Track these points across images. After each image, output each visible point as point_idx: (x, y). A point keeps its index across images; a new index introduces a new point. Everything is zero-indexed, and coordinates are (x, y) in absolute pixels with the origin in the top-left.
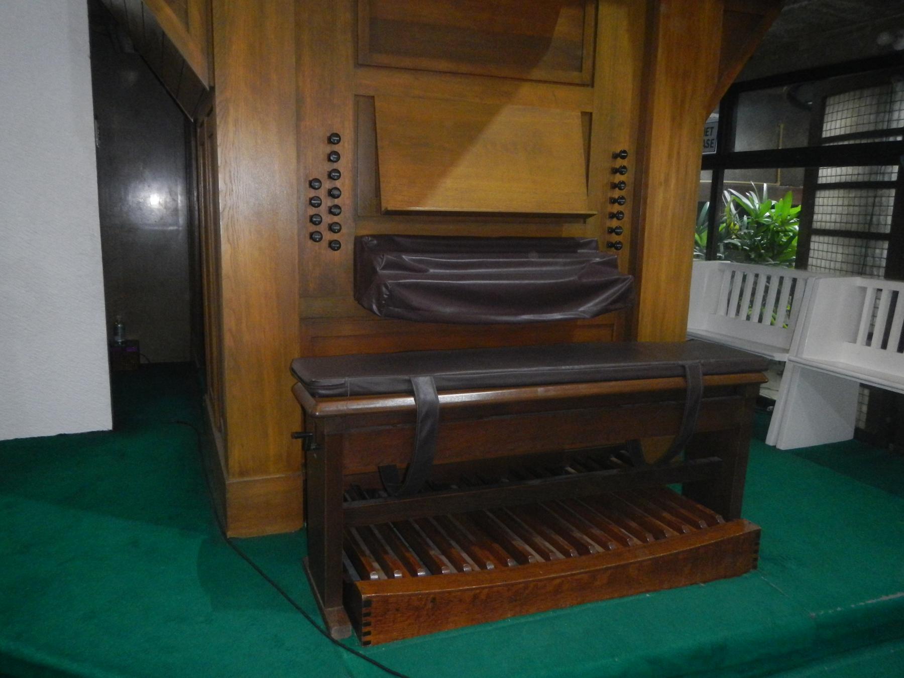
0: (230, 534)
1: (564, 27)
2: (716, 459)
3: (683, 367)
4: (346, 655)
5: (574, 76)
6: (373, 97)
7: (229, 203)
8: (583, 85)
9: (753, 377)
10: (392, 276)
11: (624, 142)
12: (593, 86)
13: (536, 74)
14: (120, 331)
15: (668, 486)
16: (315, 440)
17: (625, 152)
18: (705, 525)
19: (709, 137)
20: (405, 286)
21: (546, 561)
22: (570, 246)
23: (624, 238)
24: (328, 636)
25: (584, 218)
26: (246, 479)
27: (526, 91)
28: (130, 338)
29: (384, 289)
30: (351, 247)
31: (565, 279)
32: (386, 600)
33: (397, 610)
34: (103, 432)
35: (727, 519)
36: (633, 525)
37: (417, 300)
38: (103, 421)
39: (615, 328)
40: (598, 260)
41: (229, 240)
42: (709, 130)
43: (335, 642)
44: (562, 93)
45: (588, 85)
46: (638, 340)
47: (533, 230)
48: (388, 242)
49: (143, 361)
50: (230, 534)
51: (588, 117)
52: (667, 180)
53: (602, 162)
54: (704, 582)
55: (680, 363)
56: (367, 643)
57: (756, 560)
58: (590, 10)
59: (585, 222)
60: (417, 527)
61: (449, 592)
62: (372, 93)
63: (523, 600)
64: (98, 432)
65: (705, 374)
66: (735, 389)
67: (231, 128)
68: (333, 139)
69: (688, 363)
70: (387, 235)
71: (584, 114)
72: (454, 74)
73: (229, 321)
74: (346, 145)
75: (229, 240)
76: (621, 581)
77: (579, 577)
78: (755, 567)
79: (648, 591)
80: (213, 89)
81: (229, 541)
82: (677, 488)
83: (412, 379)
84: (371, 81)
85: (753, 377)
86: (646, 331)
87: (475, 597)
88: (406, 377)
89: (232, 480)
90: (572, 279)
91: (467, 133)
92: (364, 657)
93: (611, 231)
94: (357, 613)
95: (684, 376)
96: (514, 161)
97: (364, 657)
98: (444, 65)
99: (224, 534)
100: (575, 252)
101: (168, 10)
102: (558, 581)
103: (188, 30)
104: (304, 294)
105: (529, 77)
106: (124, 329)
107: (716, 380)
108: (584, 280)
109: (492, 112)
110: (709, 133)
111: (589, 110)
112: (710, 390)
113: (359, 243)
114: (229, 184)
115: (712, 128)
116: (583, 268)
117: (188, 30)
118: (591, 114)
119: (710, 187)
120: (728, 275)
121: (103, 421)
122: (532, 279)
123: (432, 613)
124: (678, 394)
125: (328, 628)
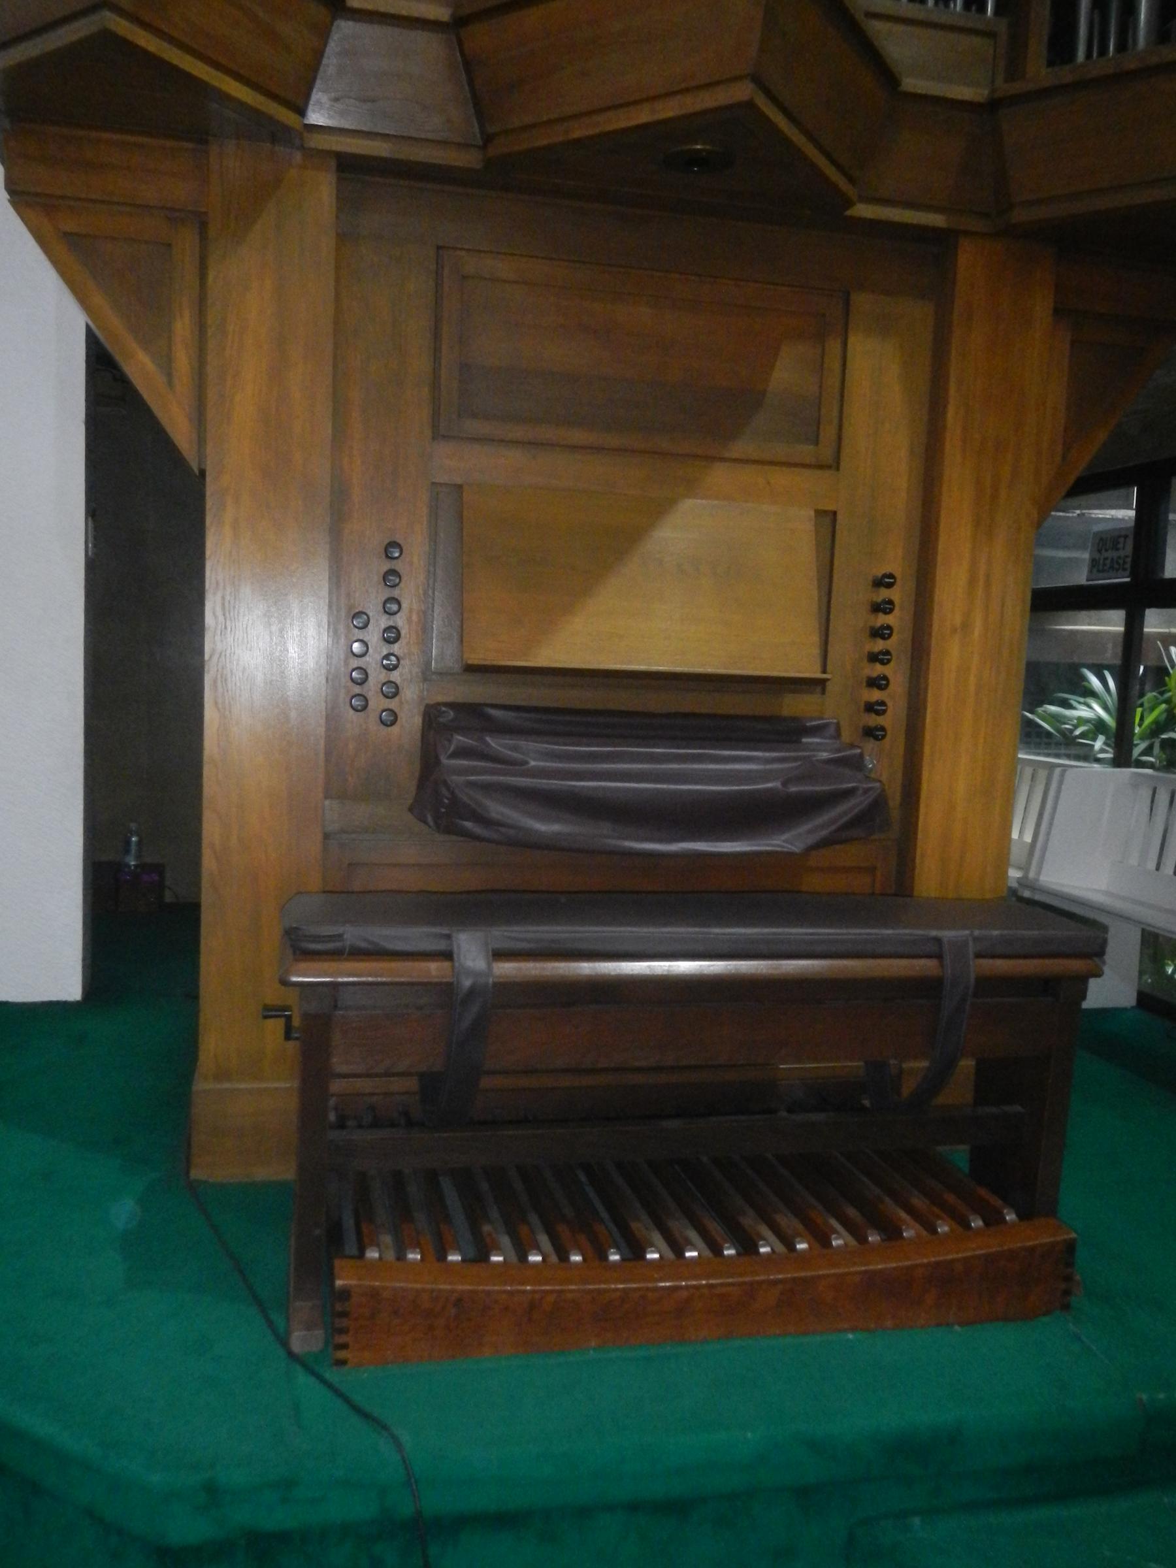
0: (195, 1174)
1: (787, 373)
2: (1018, 1108)
3: (938, 940)
4: (303, 1379)
5: (805, 451)
6: (460, 487)
7: (219, 647)
8: (821, 467)
9: (1076, 965)
10: (503, 769)
11: (895, 559)
12: (838, 469)
13: (738, 448)
14: (133, 848)
15: (940, 1149)
16: (314, 1030)
17: (891, 576)
18: (980, 1223)
19: (1122, 553)
20: (487, 788)
21: (678, 1260)
22: (787, 733)
23: (893, 719)
24: (284, 1342)
25: (817, 685)
26: (227, 1085)
27: (719, 476)
28: (148, 860)
29: (444, 791)
30: (418, 720)
31: (788, 789)
32: (374, 1294)
33: (395, 1312)
34: (66, 1003)
35: (1025, 1215)
36: (852, 1212)
37: (497, 809)
38: (70, 989)
39: (879, 873)
40: (825, 755)
41: (216, 703)
42: (1122, 540)
43: (291, 1354)
44: (782, 479)
45: (829, 467)
46: (916, 893)
47: (622, 700)
48: (472, 715)
49: (168, 898)
50: (195, 1174)
51: (828, 520)
52: (966, 626)
53: (853, 596)
54: (961, 1324)
55: (934, 933)
56: (341, 1363)
57: (1067, 1293)
58: (834, 346)
59: (823, 692)
60: (485, 1186)
61: (488, 1293)
62: (459, 481)
63: (617, 1319)
64: (58, 1003)
65: (979, 955)
66: (1047, 985)
67: (227, 530)
68: (391, 547)
69: (947, 934)
70: (471, 705)
71: (820, 513)
72: (598, 449)
73: (211, 830)
74: (415, 559)
75: (216, 703)
76: (800, 1305)
77: (724, 1290)
78: (1066, 1307)
79: (853, 1329)
80: (203, 473)
81: (193, 1187)
82: (959, 1156)
83: (454, 935)
84: (454, 462)
85: (1076, 965)
86: (929, 879)
87: (533, 1306)
88: (445, 931)
89: (202, 1085)
90: (770, 785)
91: (609, 545)
92: (329, 1385)
93: (870, 708)
94: (340, 1317)
95: (939, 957)
96: (699, 590)
97: (329, 1385)
98: (578, 436)
99: (188, 1173)
100: (798, 741)
101: (143, 357)
102: (685, 1294)
103: (170, 383)
104: (336, 789)
105: (727, 455)
106: (139, 843)
107: (1002, 966)
108: (793, 789)
109: (658, 510)
110: (1121, 546)
111: (831, 508)
112: (988, 985)
113: (431, 715)
114: (221, 618)
115: (1126, 537)
116: (797, 768)
117: (170, 383)
118: (835, 513)
119: (1121, 640)
120: (1146, 794)
121: (70, 989)
122: (696, 783)
123: (457, 1325)
124: (929, 987)
125: (288, 1333)
